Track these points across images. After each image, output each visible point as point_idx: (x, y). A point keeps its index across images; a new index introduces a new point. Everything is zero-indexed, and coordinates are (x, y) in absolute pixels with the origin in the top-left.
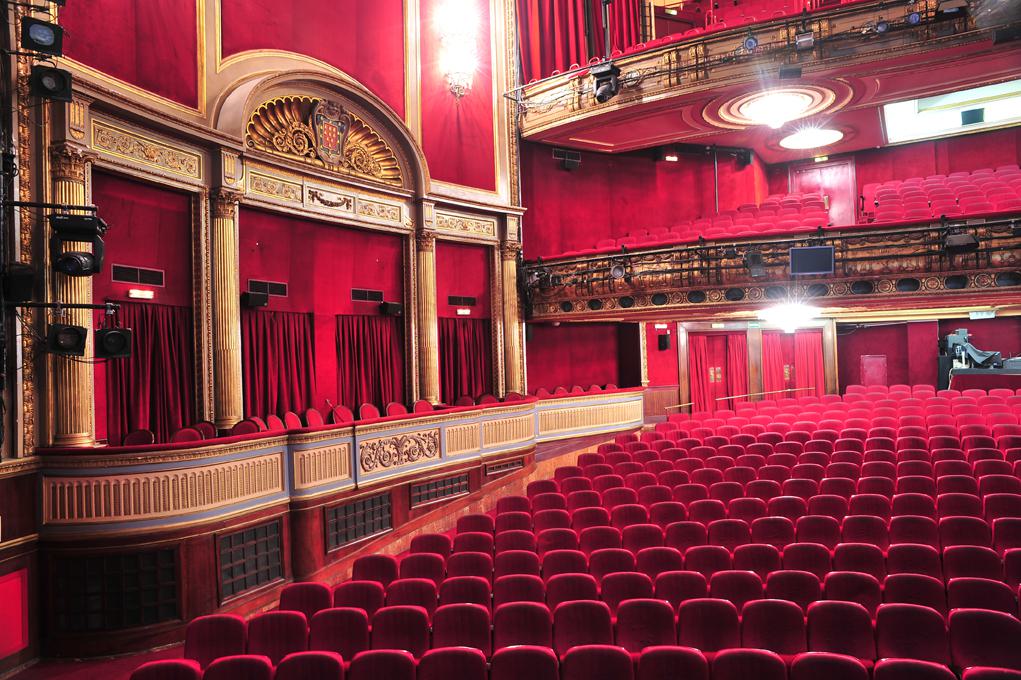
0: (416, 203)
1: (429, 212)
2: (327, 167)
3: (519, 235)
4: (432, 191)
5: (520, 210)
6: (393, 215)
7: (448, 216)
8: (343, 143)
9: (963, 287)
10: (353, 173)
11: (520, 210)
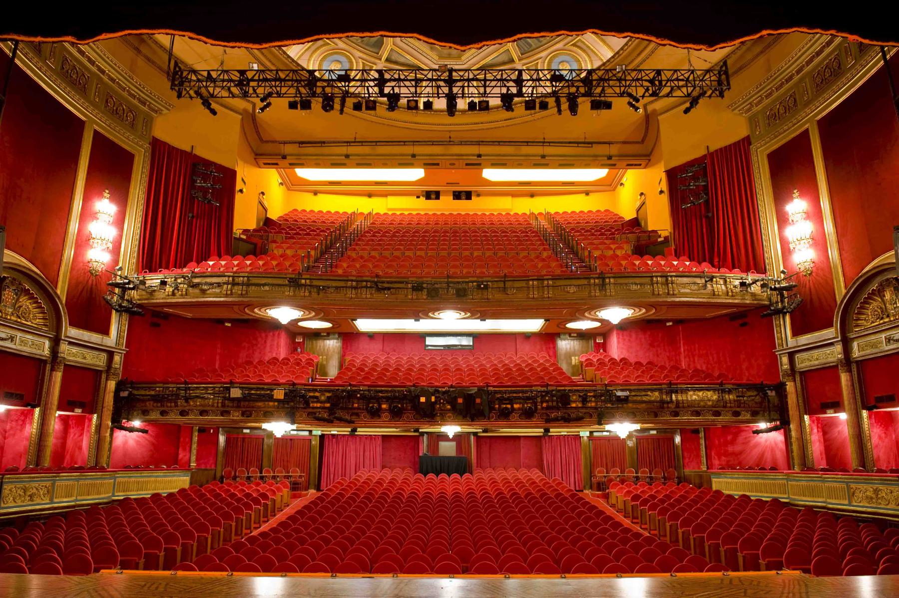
0: (56, 342)
1: (64, 347)
2: (4, 316)
3: (120, 365)
4: (68, 335)
5: (123, 350)
6: (44, 348)
7: (74, 350)
8: (16, 302)
9: (719, 416)
10: (19, 320)
11: (123, 350)
